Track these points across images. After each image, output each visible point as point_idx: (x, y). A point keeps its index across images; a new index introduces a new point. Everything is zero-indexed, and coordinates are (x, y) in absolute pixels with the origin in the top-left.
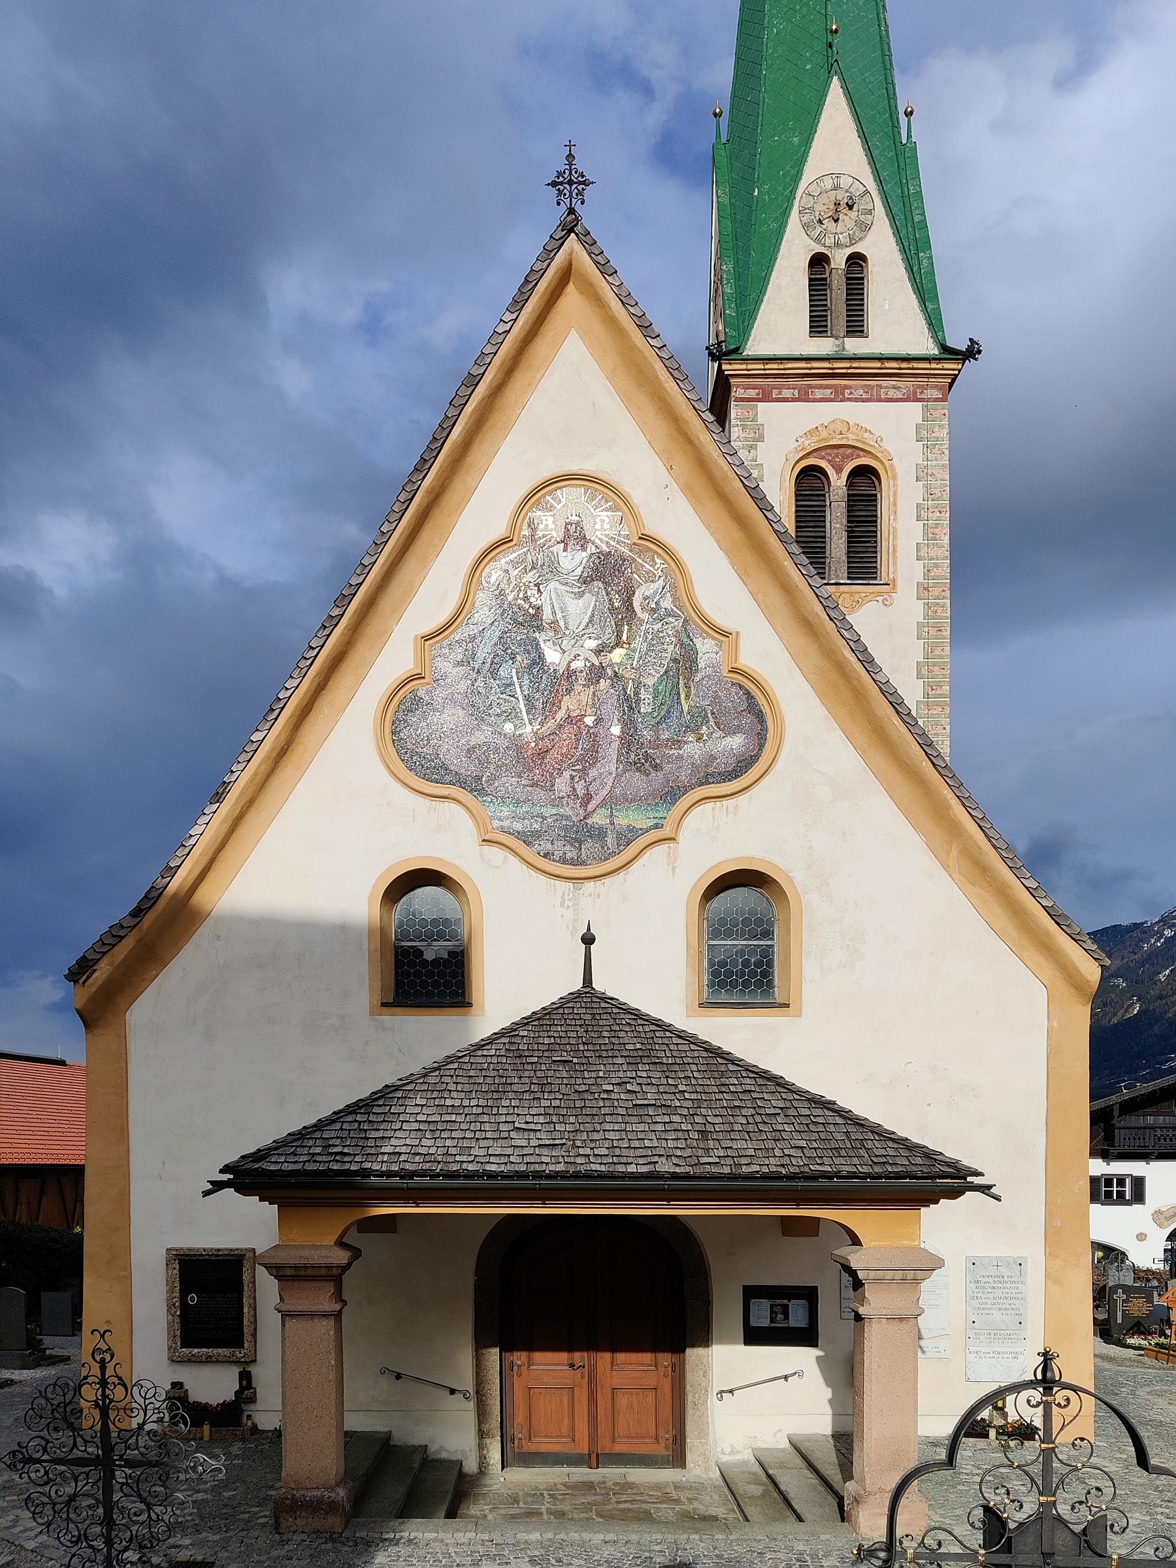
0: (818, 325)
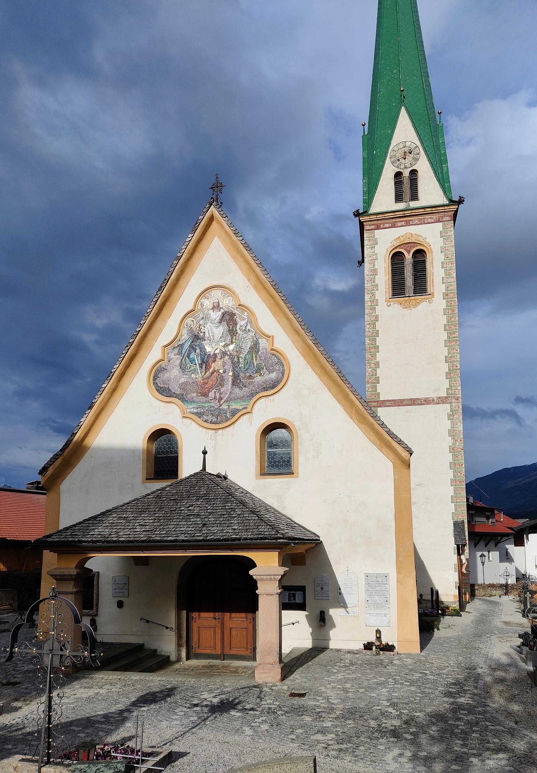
0: (399, 198)
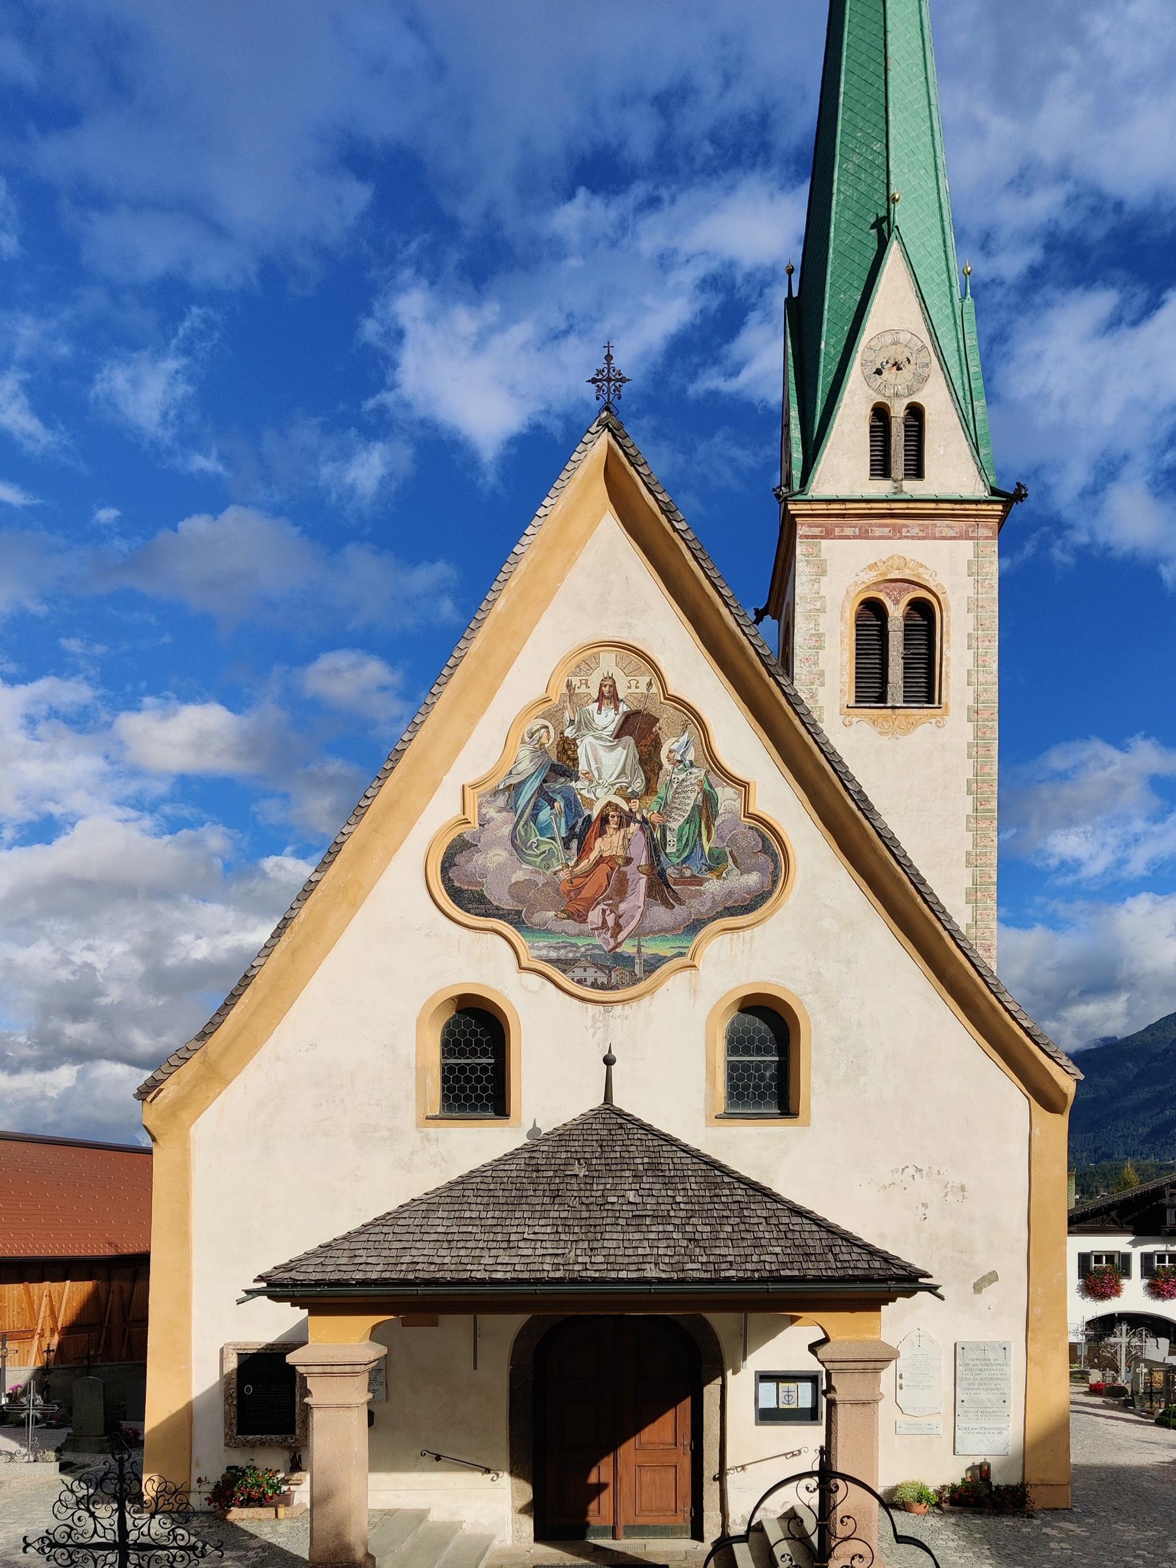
0: (881, 467)
